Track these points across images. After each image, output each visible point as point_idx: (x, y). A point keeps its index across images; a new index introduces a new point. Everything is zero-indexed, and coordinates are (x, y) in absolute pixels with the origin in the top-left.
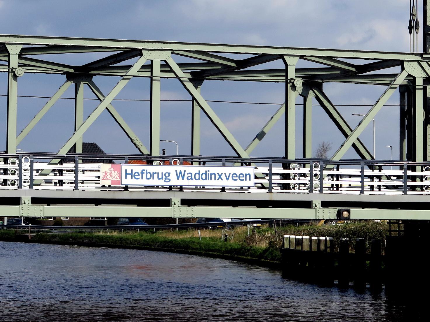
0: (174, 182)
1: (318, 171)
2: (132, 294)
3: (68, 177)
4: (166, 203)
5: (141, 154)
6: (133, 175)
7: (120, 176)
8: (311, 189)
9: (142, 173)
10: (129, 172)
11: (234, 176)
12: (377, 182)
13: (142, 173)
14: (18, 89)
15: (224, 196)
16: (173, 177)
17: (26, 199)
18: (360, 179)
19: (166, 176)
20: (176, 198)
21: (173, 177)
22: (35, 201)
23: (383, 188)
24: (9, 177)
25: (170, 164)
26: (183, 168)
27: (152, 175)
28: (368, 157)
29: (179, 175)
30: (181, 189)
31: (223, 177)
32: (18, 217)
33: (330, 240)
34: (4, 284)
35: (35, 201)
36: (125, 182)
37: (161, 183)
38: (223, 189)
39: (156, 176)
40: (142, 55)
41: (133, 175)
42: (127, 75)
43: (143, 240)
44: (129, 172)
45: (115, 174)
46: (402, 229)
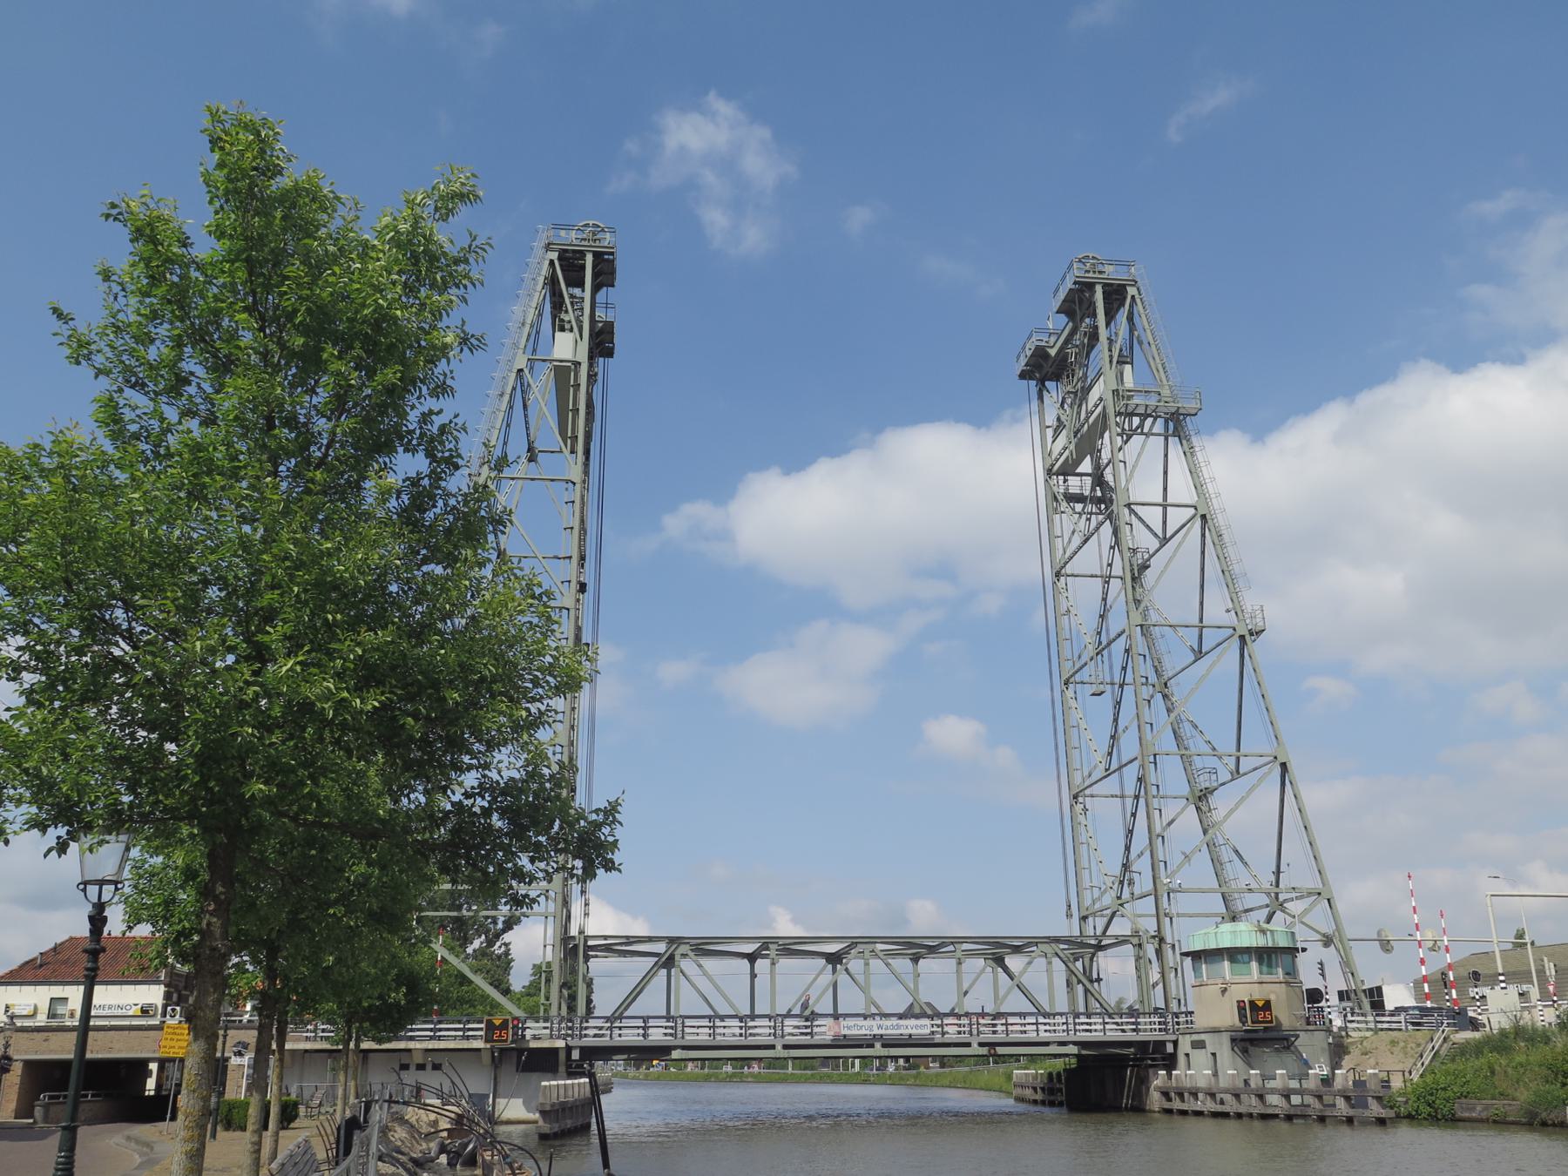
0: (876, 1031)
1: (463, 791)
2: (959, 1025)
3: (1000, 1028)
6: (849, 1028)
8: (971, 1033)
11: (916, 1026)
12: (619, 794)
16: (875, 1028)
18: (1034, 1027)
19: (871, 1028)
21: (875, 1028)
22: (786, 1047)
23: (1090, 835)
24: (962, 1029)
25: (459, 971)
26: (881, 1022)
28: (1042, 1011)
29: (880, 1027)
35: (786, 1047)
41: (849, 1028)
42: (1112, 636)
45: (836, 1027)
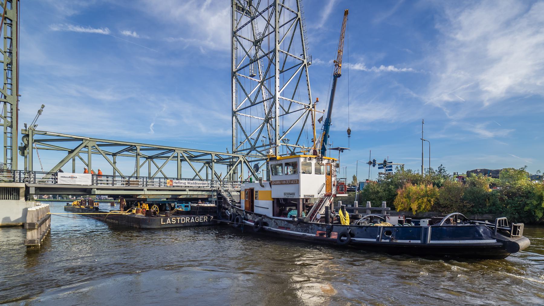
0: (187, 185)
4: (185, 190)
5: (140, 164)
7: (172, 183)
9: (178, 182)
10: (175, 182)
13: (178, 182)
14: (396, 255)
15: (199, 189)
16: (187, 183)
17: (145, 189)
19: (185, 183)
20: (187, 190)
21: (187, 183)
22: (148, 190)
27: (181, 183)
29: (188, 183)
30: (189, 187)
31: (200, 184)
32: (273, 202)
33: (39, 248)
34: (450, 176)
36: (174, 185)
37: (184, 185)
38: (199, 187)
39: (182, 183)
40: (175, 151)
43: (542, 195)
44: (175, 182)
46: (440, 203)
